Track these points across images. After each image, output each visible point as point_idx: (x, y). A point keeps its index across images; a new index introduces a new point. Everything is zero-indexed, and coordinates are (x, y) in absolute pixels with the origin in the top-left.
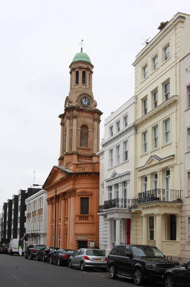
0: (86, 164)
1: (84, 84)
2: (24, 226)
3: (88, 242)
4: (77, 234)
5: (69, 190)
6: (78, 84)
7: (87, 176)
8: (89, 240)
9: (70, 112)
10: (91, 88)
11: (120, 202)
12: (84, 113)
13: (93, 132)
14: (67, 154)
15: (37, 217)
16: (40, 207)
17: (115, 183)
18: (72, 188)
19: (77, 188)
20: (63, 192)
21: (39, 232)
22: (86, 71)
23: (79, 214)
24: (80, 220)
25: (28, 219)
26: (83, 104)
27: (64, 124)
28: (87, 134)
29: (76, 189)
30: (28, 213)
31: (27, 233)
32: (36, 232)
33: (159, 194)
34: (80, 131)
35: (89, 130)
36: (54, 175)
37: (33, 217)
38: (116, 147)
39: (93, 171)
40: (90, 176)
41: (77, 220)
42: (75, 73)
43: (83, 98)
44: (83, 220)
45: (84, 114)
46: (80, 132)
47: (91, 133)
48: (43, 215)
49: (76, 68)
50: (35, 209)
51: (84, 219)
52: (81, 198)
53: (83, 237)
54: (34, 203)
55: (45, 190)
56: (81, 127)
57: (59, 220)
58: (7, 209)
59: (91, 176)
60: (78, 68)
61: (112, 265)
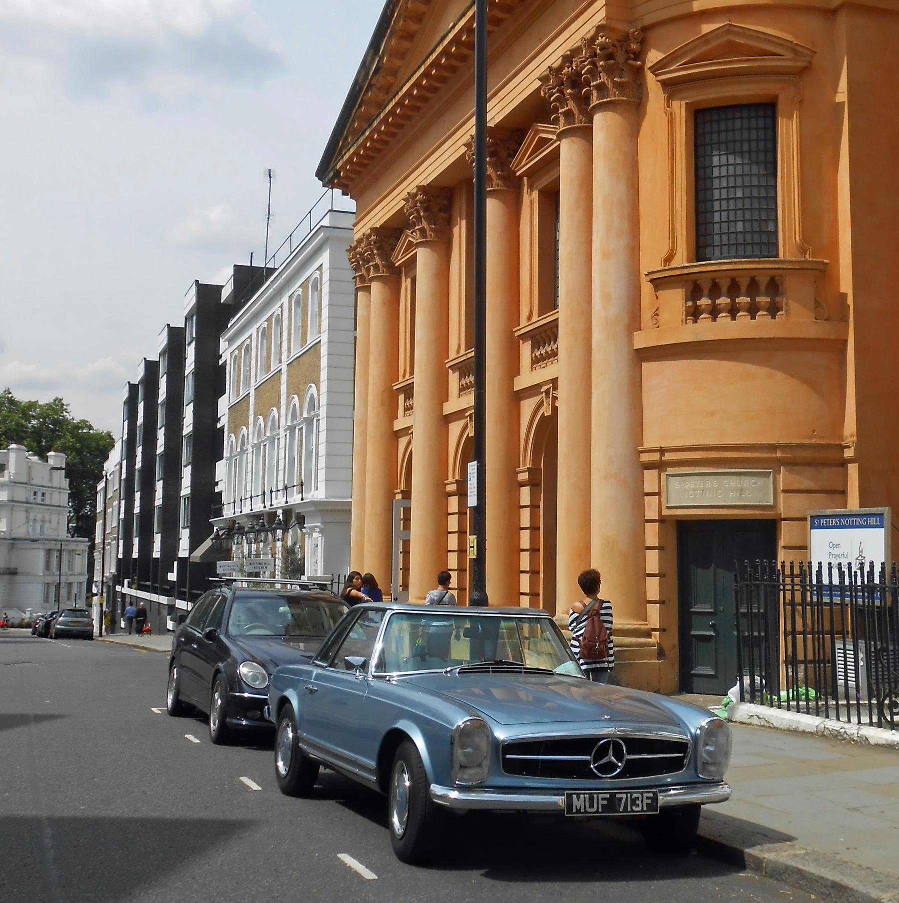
0: (14, 664)
2: (217, 484)
3: (786, 535)
4: (668, 457)
16: (304, 341)
19: (648, 20)
21: (295, 499)
23: (681, 260)
24: (694, 314)
29: (645, 29)
30: (234, 400)
31: (228, 513)
32: (279, 502)
41: (664, 317)
44: (724, 319)
48: (324, 386)
50: (273, 368)
51: (723, 301)
53: (731, 482)
57: (401, 398)
58: (153, 542)
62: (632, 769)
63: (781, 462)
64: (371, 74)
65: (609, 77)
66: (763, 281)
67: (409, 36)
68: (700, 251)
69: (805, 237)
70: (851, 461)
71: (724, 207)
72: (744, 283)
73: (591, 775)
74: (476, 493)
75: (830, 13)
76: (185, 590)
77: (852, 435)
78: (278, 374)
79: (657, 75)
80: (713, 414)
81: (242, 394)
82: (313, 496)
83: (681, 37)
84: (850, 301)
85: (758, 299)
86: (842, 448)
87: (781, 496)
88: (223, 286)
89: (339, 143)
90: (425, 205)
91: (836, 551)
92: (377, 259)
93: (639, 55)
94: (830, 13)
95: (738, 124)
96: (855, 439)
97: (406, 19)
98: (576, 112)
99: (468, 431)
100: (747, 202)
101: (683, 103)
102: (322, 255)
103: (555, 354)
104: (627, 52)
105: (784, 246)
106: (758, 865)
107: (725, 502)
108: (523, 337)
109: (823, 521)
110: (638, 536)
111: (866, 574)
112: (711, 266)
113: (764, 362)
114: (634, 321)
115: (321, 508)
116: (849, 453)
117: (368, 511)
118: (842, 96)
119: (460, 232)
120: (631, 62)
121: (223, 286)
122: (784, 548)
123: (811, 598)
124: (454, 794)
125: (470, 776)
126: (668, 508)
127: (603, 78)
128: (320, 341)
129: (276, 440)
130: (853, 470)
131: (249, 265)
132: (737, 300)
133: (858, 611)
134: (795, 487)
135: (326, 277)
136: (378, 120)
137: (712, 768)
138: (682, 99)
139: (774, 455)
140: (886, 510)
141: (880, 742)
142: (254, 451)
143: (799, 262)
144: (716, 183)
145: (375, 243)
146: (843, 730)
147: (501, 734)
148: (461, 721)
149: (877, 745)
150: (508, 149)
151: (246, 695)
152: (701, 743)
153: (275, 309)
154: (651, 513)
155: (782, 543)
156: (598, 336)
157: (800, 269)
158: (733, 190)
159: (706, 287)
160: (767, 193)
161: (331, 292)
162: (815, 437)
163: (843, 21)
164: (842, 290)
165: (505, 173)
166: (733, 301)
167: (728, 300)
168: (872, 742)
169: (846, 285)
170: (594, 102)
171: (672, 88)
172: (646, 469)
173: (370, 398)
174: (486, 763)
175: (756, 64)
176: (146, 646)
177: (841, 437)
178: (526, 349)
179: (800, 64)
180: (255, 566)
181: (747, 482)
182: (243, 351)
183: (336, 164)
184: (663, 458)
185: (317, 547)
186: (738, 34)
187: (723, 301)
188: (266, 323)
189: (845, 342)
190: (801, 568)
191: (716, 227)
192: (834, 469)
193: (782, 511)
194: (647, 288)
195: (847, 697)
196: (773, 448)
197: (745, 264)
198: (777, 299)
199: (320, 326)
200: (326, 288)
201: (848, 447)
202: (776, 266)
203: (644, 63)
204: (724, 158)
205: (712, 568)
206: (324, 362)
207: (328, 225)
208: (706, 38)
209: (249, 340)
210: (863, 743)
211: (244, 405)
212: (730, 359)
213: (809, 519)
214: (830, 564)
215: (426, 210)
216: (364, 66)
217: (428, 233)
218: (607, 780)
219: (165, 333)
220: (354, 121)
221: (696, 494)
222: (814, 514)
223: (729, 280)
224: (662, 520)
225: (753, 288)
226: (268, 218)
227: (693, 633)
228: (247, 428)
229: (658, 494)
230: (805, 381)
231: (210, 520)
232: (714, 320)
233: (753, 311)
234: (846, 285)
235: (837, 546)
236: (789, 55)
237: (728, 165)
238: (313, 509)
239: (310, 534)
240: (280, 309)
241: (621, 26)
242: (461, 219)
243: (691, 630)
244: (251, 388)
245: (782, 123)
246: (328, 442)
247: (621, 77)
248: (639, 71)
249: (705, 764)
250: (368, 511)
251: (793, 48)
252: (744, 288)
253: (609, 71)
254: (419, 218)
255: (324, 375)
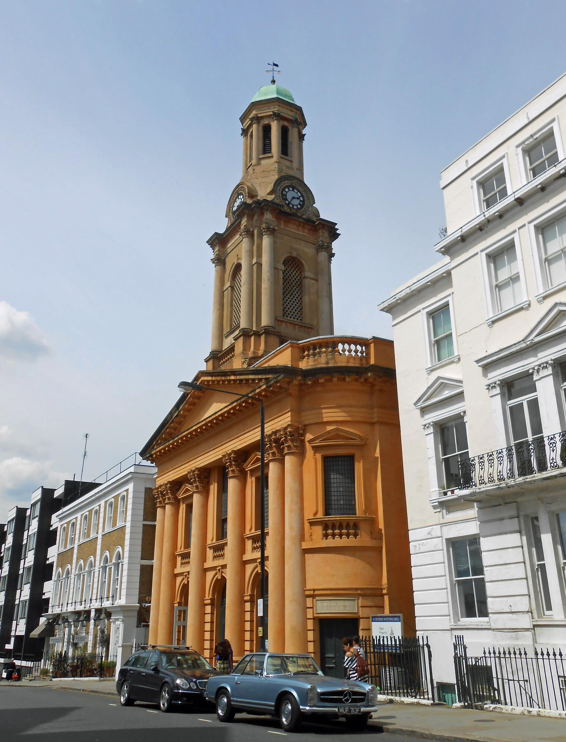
1: (286, 157)
3: (362, 624)
4: (316, 592)
5: (279, 431)
6: (269, 155)
7: (347, 379)
8: (362, 613)
9: (252, 219)
10: (301, 168)
11: (477, 466)
12: (291, 225)
13: (317, 280)
14: (246, 334)
15: (98, 557)
16: (114, 524)
17: (501, 378)
18: (289, 423)
19: (306, 422)
20: (239, 447)
21: (107, 604)
22: (290, 128)
23: (320, 515)
24: (326, 536)
25: (60, 569)
26: (287, 202)
27: (224, 260)
28: (300, 285)
29: (305, 426)
30: (62, 550)
33: (553, 451)
34: (281, 272)
35: (307, 274)
36: (193, 404)
37: (107, 553)
38: (535, 226)
39: (362, 365)
40: (356, 380)
41: (314, 537)
42: (261, 129)
43: (288, 187)
45: (292, 228)
46: (281, 275)
47: (313, 281)
48: (127, 548)
49: (262, 118)
50: (92, 535)
51: (337, 531)
52: (326, 459)
53: (341, 603)
54: (113, 506)
55: (148, 463)
56: (285, 263)
59: (362, 380)
60: (269, 116)
61: (222, 696)
62: (354, 701)
63: (359, 595)
64: (174, 417)
65: (292, 443)
66: (351, 524)
67: (193, 404)
68: (327, 512)
69: (366, 508)
70: (385, 594)
71: (336, 494)
72: (344, 524)
73: (343, 702)
74: (262, 611)
75: (373, 424)
76: (20, 654)
77: (385, 584)
78: (95, 539)
79: (310, 444)
80: (333, 576)
81: (69, 547)
82: (118, 603)
83: (320, 431)
84: (383, 532)
85: (350, 531)
86: (382, 589)
87: (360, 609)
88: (56, 490)
89: (153, 442)
90: (199, 476)
91: (382, 631)
92: (170, 494)
93: (303, 435)
94: (373, 424)
95: (340, 463)
96: (387, 586)
97: (193, 398)
98: (276, 452)
99: (217, 576)
100: (344, 493)
101: (320, 455)
102: (128, 485)
103: (223, 555)
104: (298, 434)
105: (359, 511)
106: (388, 730)
107: (339, 611)
108: (248, 538)
109: (376, 619)
110: (305, 625)
111: (377, 640)
112: (332, 517)
113: (353, 555)
114: (302, 538)
115: (123, 609)
116: (385, 591)
117: (161, 612)
118: (378, 454)
119: (214, 488)
120: (300, 437)
121: (56, 490)
122: (362, 630)
123: (370, 650)
124: (308, 708)
125: (312, 703)
126: (317, 613)
127: (290, 443)
128: (126, 526)
129: (92, 573)
130: (386, 598)
131: (73, 480)
132: (342, 531)
133: (390, 654)
134: (365, 605)
135: (131, 495)
136: (178, 438)
137: (373, 701)
138: (319, 453)
139: (357, 592)
140: (401, 615)
141: (408, 702)
142: (76, 578)
143: (365, 517)
144: (332, 485)
145: (169, 488)
146: (394, 699)
147: (319, 690)
148: (309, 686)
149: (407, 704)
150: (242, 459)
151: (180, 691)
152: (370, 694)
153: (95, 506)
154: (310, 615)
155: (361, 628)
156: (287, 543)
157: (365, 520)
158: (339, 488)
159: (330, 526)
160: (348, 485)
161: (133, 503)
162: (372, 585)
163: (377, 427)
164: (380, 527)
165: (240, 469)
166: (341, 531)
167: (339, 531)
168: (405, 703)
169: (381, 525)
170: (286, 451)
171: (316, 449)
172: (308, 597)
173: (164, 558)
174: (316, 699)
175: (347, 442)
176: (20, 685)
177: (381, 585)
178: (179, 559)
179: (363, 443)
180: (79, 639)
181: (347, 603)
182: (70, 525)
183: (152, 452)
184: (314, 593)
185: (118, 629)
186: (340, 431)
187: (337, 531)
188: (88, 513)
189: (382, 548)
190: (369, 638)
191: (333, 502)
192: (379, 598)
193: (361, 615)
194: (307, 525)
195: (391, 689)
196: (357, 589)
197: (345, 517)
198: (357, 531)
199: (126, 518)
200: (130, 501)
201: (384, 589)
202: (355, 519)
203: (305, 438)
204: (335, 476)
205: (334, 638)
206: (127, 536)
207: (133, 471)
208: (329, 432)
209: (75, 520)
210: (402, 703)
211: (69, 553)
212: (340, 554)
213: (371, 618)
214: (380, 636)
215: (198, 478)
216: (171, 413)
217: (200, 487)
218: (348, 704)
219: (15, 510)
220: (162, 434)
221: (327, 608)
222: (373, 616)
223: (339, 523)
224: (314, 619)
225: (348, 527)
226: (84, 457)
227: (327, 666)
228: (71, 565)
229: (312, 608)
230: (368, 563)
231: (42, 614)
232: (334, 539)
233: (348, 535)
234: (381, 525)
235: (383, 629)
236: (359, 440)
237: (337, 478)
238: (119, 609)
239: (114, 622)
240: (98, 507)
241: (296, 424)
242: (215, 483)
243: (325, 665)
244: (75, 545)
245: (356, 464)
246: (128, 576)
247: (296, 443)
248: (303, 441)
249: (371, 700)
250: (161, 612)
251: (361, 438)
252: (344, 527)
253: (292, 440)
254: (195, 481)
255: (127, 542)
